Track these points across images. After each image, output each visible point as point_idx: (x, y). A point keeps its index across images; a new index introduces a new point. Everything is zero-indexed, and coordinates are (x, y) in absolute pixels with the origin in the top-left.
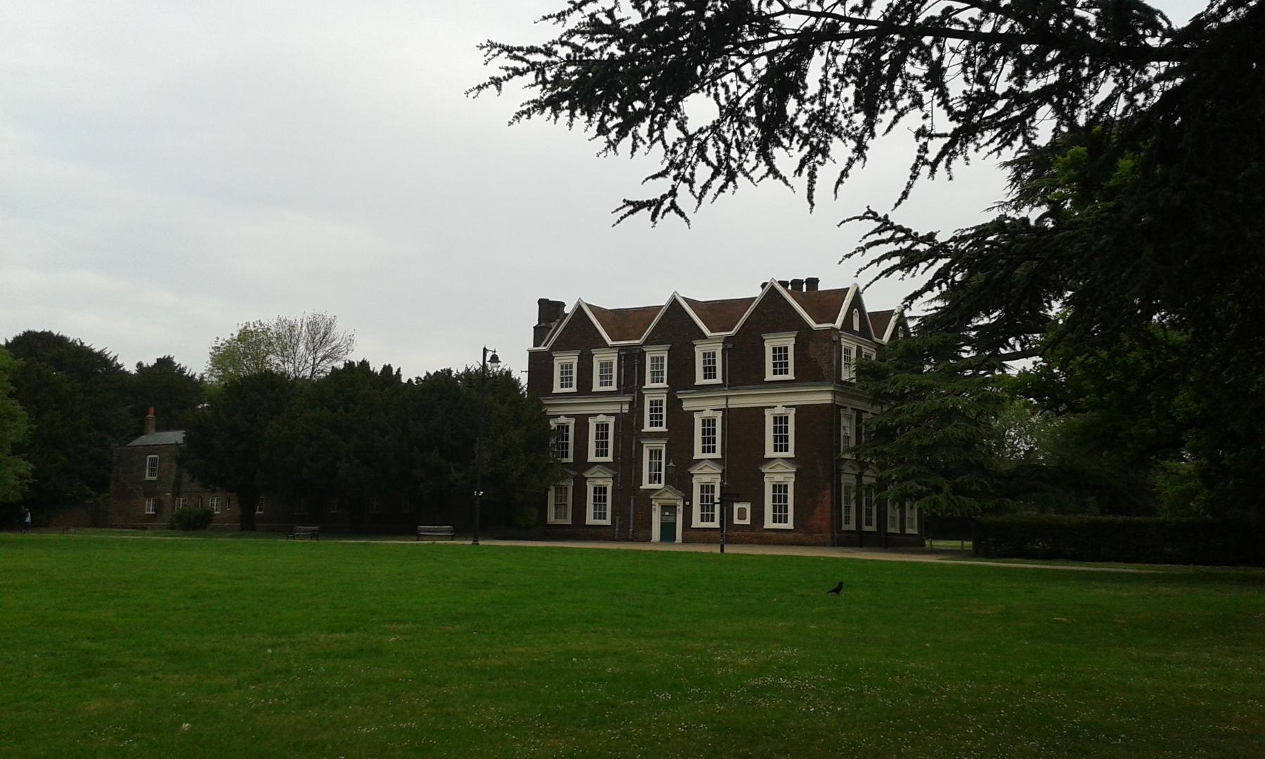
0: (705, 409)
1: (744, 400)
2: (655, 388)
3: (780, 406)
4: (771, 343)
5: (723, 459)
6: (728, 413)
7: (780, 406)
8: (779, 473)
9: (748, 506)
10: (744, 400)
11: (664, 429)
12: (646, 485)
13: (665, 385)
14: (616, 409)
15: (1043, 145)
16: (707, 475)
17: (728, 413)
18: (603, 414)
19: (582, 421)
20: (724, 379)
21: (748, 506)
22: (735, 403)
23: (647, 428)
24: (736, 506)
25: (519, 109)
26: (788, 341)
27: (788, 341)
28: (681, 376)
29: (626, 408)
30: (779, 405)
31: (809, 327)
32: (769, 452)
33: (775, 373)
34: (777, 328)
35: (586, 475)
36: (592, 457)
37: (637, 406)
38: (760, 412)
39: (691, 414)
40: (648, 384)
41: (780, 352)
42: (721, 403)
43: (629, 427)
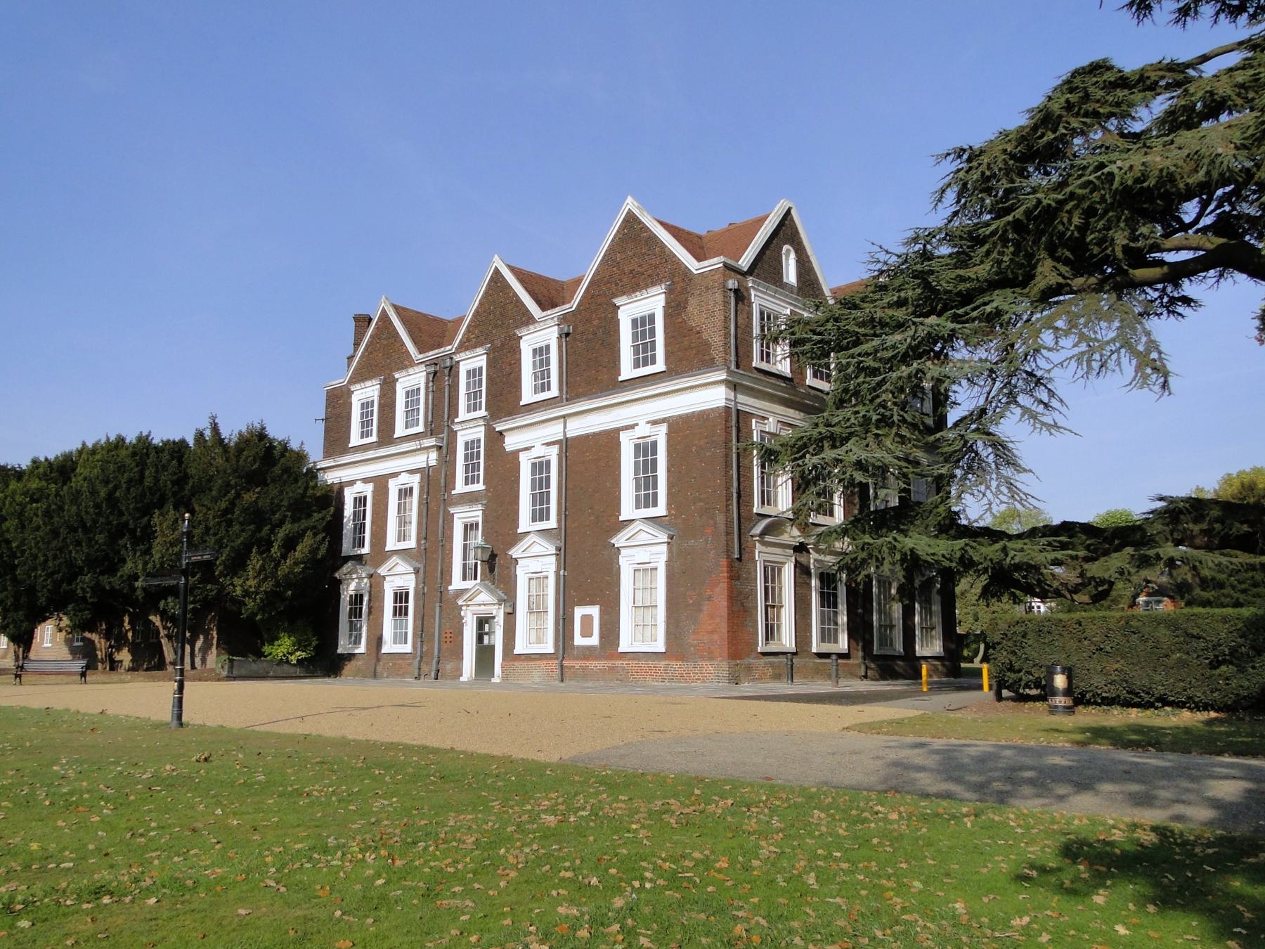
0: (534, 442)
1: (589, 421)
2: (470, 429)
3: (642, 423)
4: (629, 310)
5: (559, 528)
6: (568, 446)
7: (642, 423)
8: (643, 554)
9: (594, 611)
10: (589, 421)
11: (480, 486)
12: (457, 583)
13: (483, 412)
14: (419, 461)
15: (38, 631)
16: (536, 561)
17: (568, 446)
18: (406, 467)
19: (380, 483)
20: (560, 389)
21: (594, 611)
22: (578, 427)
23: (460, 487)
24: (579, 612)
25: (941, 184)
26: (652, 302)
27: (652, 302)
28: (503, 397)
29: (433, 456)
30: (642, 417)
31: (686, 272)
32: (628, 509)
33: (637, 365)
34: (636, 284)
35: (382, 571)
36: (391, 544)
37: (447, 451)
38: (608, 442)
39: (516, 454)
40: (463, 414)
41: (643, 325)
42: (555, 431)
43: (436, 486)
